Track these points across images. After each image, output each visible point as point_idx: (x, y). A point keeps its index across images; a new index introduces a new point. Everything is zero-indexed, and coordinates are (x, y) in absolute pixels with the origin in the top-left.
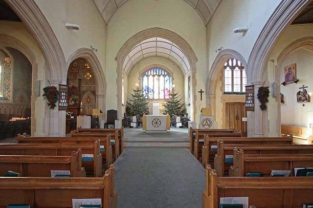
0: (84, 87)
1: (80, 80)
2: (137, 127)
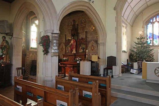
0: (90, 37)
1: (86, 32)
2: (138, 74)
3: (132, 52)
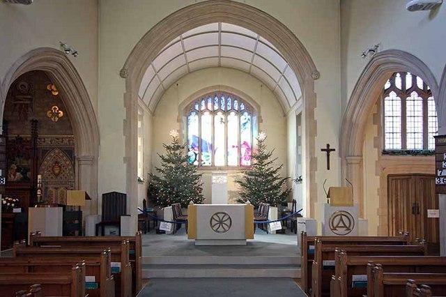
0: (46, 138)
1: (35, 123)
2: (174, 233)
3: (155, 182)
